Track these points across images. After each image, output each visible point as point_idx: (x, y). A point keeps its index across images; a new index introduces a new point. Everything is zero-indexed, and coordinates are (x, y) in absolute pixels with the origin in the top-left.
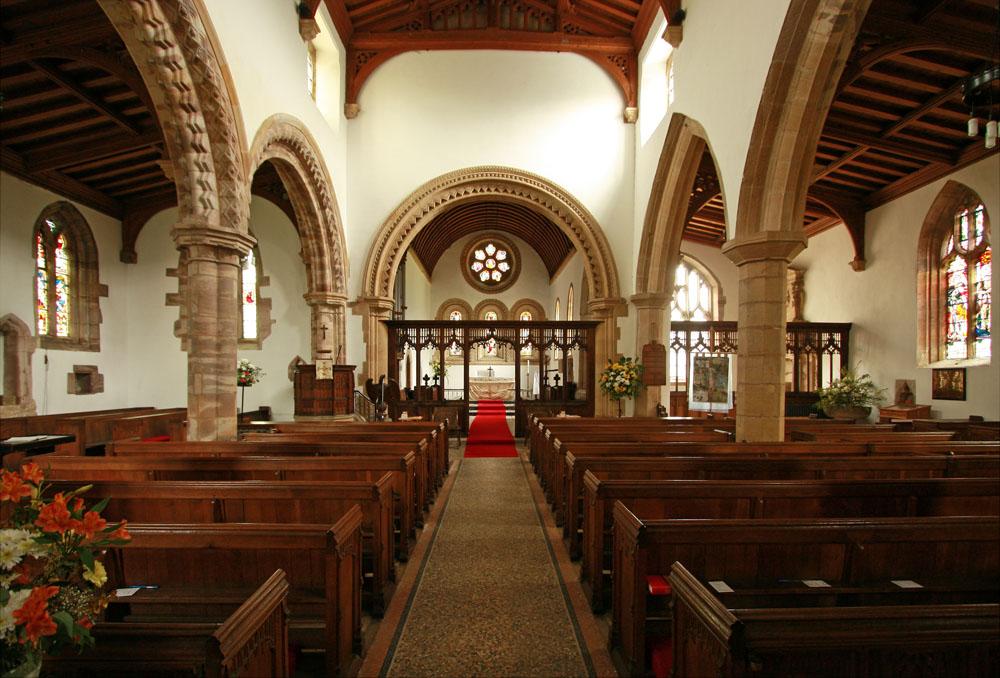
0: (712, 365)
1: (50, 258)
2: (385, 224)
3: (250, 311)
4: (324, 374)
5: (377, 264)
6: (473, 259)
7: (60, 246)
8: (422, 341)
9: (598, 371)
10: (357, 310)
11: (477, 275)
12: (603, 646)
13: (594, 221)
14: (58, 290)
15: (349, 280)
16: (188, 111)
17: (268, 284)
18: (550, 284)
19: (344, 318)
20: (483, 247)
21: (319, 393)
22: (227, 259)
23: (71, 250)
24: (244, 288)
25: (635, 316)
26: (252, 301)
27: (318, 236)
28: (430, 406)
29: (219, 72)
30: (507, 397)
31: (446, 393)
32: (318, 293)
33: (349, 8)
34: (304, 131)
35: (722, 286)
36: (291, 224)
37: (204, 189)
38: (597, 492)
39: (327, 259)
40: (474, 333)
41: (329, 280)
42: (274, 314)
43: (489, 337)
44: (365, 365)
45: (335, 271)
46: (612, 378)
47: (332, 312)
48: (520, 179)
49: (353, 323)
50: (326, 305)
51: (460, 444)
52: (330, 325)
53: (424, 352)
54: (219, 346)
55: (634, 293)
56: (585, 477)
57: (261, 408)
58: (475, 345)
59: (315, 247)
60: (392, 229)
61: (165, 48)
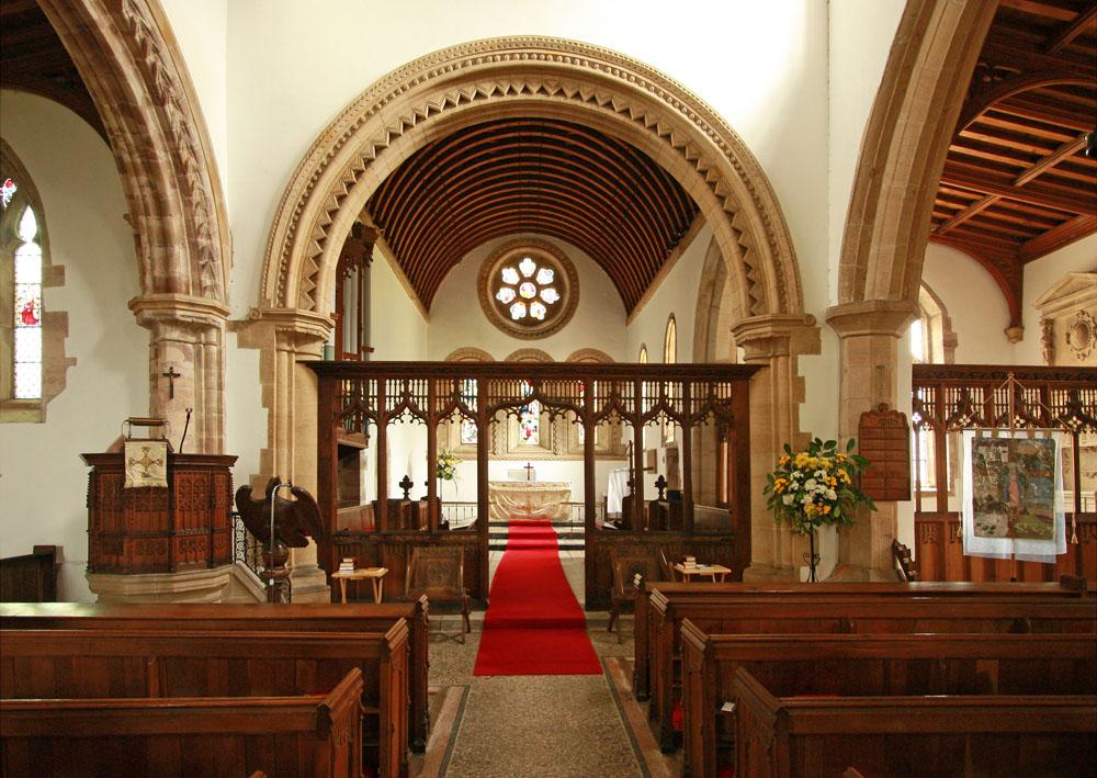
0: (1014, 457)
2: (309, 155)
3: (29, 342)
4: (146, 476)
5: (292, 240)
6: (499, 283)
8: (390, 406)
9: (756, 468)
11: (505, 309)
12: (644, 720)
13: (751, 161)
15: (231, 274)
17: (62, 283)
18: (627, 324)
19: (220, 352)
20: (514, 263)
21: (138, 520)
25: (835, 357)
26: (35, 321)
27: (151, 167)
28: (406, 544)
30: (557, 515)
31: (444, 509)
32: (156, 297)
35: (950, 315)
36: (104, 143)
38: (705, 652)
39: (176, 223)
40: (498, 389)
41: (182, 268)
42: (71, 347)
43: (529, 400)
44: (266, 455)
45: (197, 252)
46: (795, 485)
47: (193, 339)
48: (592, 65)
49: (239, 365)
50: (175, 323)
51: (468, 627)
52: (186, 369)
53: (394, 430)
55: (835, 303)
56: (683, 629)
57: (36, 548)
58: (500, 414)
59: (147, 191)
60: (324, 167)
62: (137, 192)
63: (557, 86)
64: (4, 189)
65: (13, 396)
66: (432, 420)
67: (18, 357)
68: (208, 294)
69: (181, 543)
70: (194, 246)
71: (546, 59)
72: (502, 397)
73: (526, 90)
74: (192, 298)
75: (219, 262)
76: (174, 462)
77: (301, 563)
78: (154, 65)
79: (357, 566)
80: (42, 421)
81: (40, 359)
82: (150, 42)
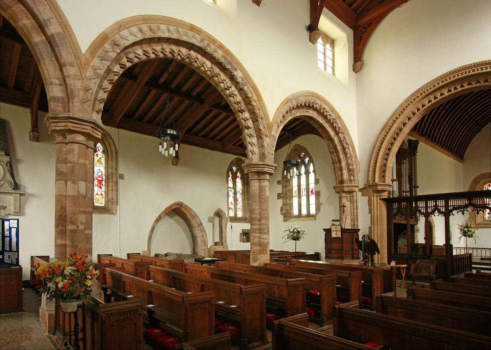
1: (234, 183)
2: (380, 134)
4: (336, 234)
5: (376, 161)
7: (237, 177)
10: (365, 194)
14: (237, 197)
15: (359, 175)
16: (242, 113)
19: (357, 198)
21: (335, 246)
22: (262, 177)
23: (242, 178)
24: (310, 187)
29: (252, 89)
31: (462, 254)
33: (350, 6)
34: (314, 95)
37: (252, 146)
39: (344, 164)
41: (346, 176)
42: (322, 200)
45: (349, 170)
47: (349, 196)
49: (362, 201)
50: (344, 192)
52: (348, 204)
54: (260, 220)
59: (336, 157)
60: (385, 136)
61: (228, 90)
62: (334, 158)
63: (475, 81)
64: (306, 159)
65: (309, 214)
66: (447, 214)
67: (310, 203)
68: (353, 182)
69: (345, 252)
70: (348, 169)
71: (469, 72)
72: (455, 206)
73: (462, 86)
74: (349, 184)
75: (355, 172)
76: (343, 231)
77: (382, 262)
78: (336, 126)
79: (397, 263)
80: (316, 220)
81: (314, 203)
82: (334, 121)
